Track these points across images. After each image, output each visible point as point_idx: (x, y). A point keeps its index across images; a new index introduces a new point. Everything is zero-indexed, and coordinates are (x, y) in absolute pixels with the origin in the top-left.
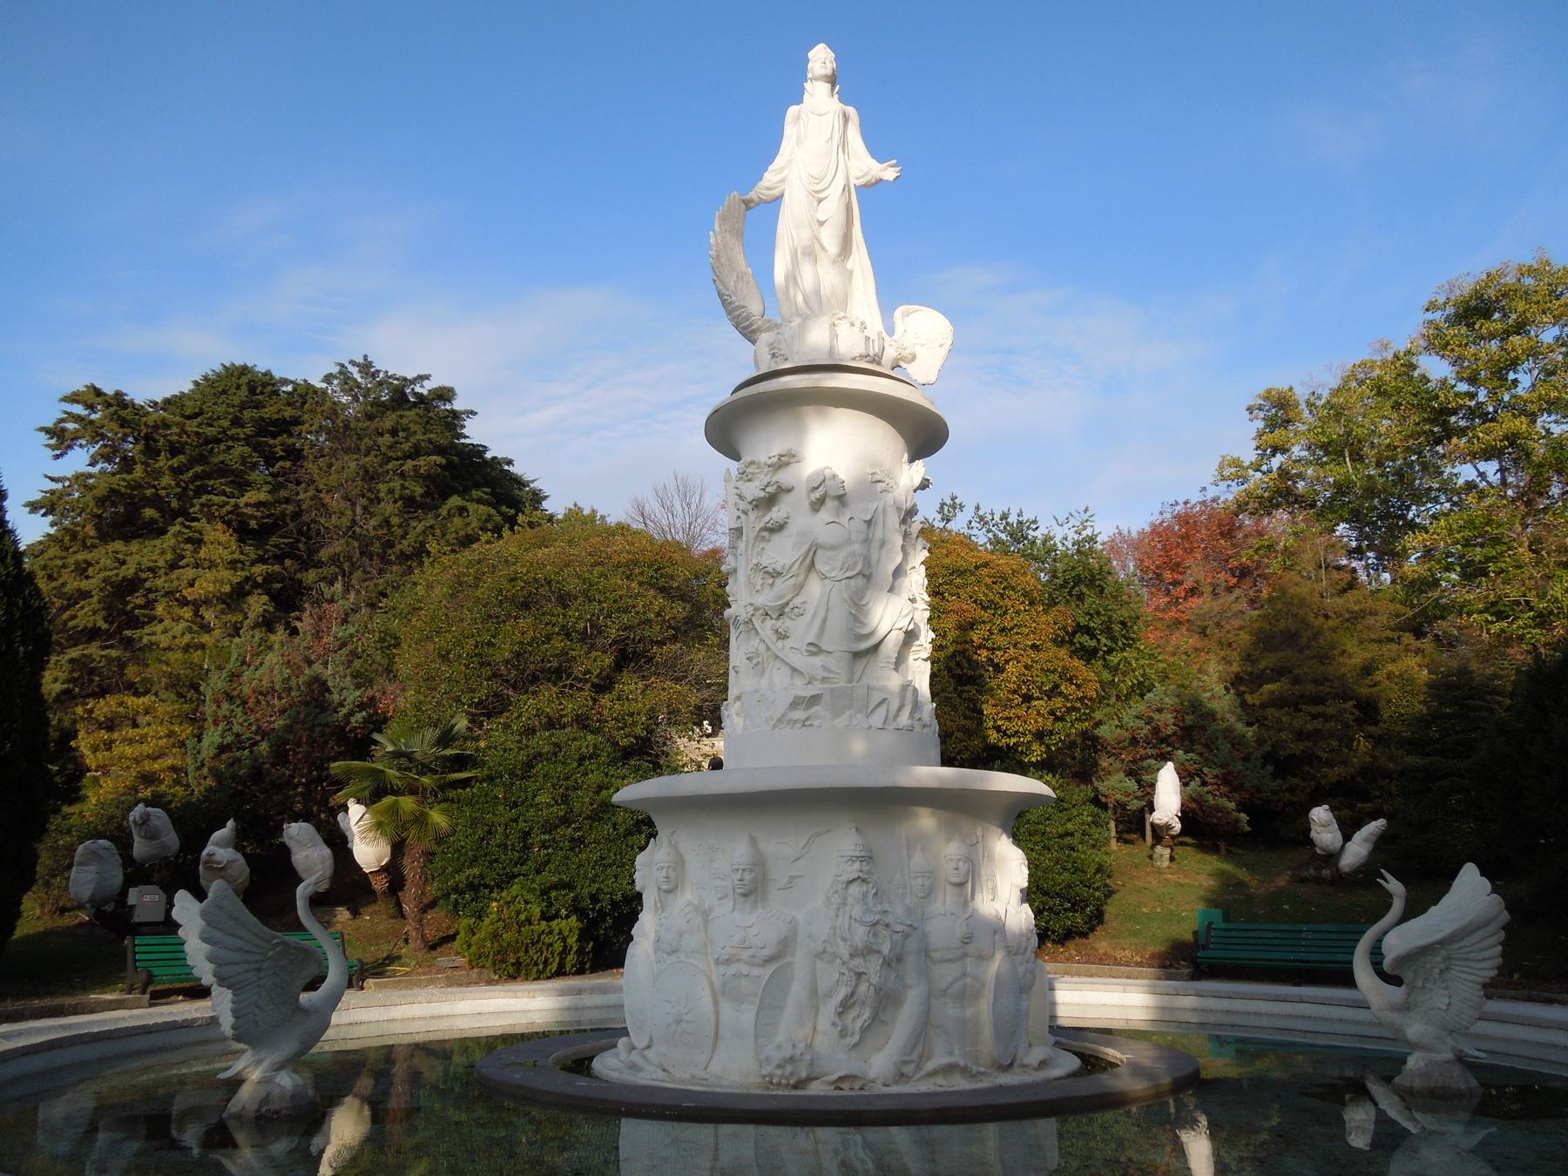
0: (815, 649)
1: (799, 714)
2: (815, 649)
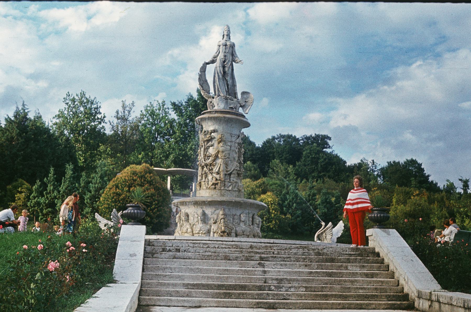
0: (218, 173)
1: (213, 187)
2: (218, 173)
